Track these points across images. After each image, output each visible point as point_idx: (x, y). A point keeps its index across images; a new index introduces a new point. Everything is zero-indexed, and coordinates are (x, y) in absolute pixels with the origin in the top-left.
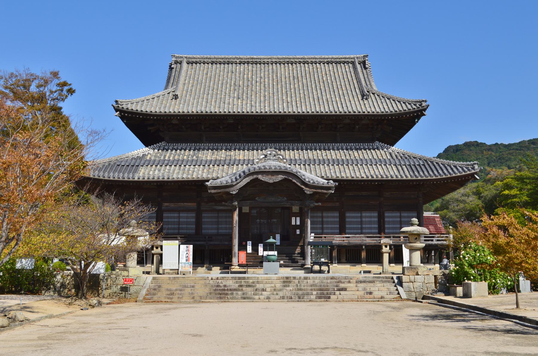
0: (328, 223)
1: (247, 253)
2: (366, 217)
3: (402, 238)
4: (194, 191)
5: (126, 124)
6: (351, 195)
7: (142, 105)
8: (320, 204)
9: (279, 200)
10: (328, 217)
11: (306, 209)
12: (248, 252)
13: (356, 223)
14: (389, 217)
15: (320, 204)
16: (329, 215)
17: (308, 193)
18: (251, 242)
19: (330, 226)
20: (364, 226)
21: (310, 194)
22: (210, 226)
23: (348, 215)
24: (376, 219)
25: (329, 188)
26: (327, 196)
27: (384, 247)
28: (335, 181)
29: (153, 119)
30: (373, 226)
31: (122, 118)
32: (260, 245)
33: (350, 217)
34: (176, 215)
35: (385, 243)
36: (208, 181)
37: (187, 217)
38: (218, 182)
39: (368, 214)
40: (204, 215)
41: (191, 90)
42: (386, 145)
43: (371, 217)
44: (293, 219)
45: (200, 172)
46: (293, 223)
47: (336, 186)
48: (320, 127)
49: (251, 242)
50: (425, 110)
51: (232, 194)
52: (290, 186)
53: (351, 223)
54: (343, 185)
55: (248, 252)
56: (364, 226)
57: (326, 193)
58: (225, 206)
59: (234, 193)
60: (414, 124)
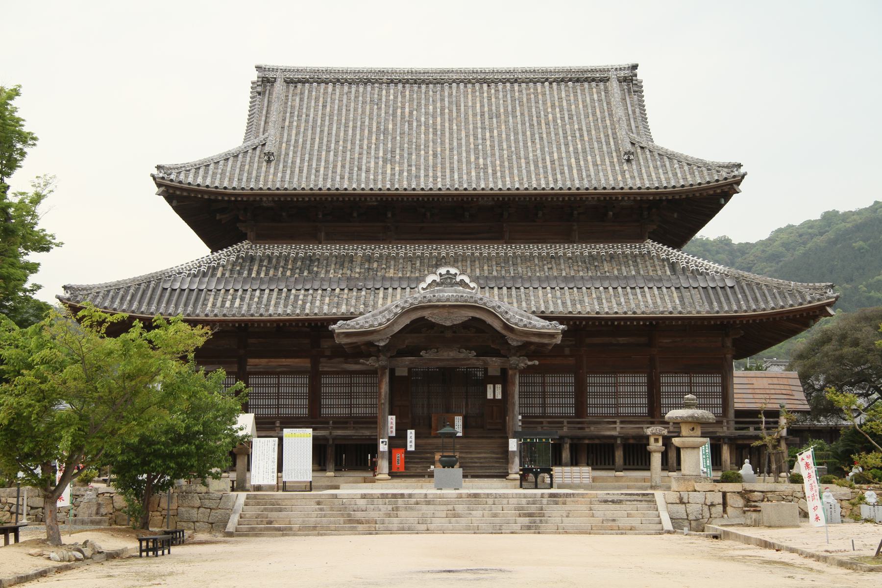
0: (553, 395)
1: (407, 452)
2: (625, 384)
3: (565, 424)
4: (306, 339)
5: (177, 209)
6: (593, 343)
7: (206, 172)
8: (537, 363)
9: (462, 356)
10: (553, 384)
11: (510, 372)
12: (409, 449)
13: (608, 395)
14: (669, 384)
15: (537, 363)
16: (557, 380)
17: (515, 344)
18: (413, 431)
19: (557, 401)
20: (621, 401)
21: (518, 347)
22: (335, 402)
23: (591, 380)
24: (644, 389)
25: (552, 336)
26: (550, 348)
27: (652, 440)
28: (561, 320)
29: (229, 201)
30: (638, 401)
31: (170, 198)
32: (409, 431)
33: (594, 385)
34: (273, 381)
35: (654, 434)
36: (335, 321)
37: (293, 386)
38: (353, 325)
39: (628, 379)
40: (324, 380)
41: (296, 141)
42: (665, 248)
43: (634, 384)
44: (490, 388)
45: (318, 303)
46: (490, 396)
47: (564, 332)
48: (540, 214)
49: (413, 431)
50: (738, 183)
51: (378, 346)
52: (480, 332)
53: (596, 395)
54: (581, 329)
55: (409, 449)
56: (621, 401)
57: (547, 344)
58: (363, 364)
59: (382, 344)
60: (720, 207)
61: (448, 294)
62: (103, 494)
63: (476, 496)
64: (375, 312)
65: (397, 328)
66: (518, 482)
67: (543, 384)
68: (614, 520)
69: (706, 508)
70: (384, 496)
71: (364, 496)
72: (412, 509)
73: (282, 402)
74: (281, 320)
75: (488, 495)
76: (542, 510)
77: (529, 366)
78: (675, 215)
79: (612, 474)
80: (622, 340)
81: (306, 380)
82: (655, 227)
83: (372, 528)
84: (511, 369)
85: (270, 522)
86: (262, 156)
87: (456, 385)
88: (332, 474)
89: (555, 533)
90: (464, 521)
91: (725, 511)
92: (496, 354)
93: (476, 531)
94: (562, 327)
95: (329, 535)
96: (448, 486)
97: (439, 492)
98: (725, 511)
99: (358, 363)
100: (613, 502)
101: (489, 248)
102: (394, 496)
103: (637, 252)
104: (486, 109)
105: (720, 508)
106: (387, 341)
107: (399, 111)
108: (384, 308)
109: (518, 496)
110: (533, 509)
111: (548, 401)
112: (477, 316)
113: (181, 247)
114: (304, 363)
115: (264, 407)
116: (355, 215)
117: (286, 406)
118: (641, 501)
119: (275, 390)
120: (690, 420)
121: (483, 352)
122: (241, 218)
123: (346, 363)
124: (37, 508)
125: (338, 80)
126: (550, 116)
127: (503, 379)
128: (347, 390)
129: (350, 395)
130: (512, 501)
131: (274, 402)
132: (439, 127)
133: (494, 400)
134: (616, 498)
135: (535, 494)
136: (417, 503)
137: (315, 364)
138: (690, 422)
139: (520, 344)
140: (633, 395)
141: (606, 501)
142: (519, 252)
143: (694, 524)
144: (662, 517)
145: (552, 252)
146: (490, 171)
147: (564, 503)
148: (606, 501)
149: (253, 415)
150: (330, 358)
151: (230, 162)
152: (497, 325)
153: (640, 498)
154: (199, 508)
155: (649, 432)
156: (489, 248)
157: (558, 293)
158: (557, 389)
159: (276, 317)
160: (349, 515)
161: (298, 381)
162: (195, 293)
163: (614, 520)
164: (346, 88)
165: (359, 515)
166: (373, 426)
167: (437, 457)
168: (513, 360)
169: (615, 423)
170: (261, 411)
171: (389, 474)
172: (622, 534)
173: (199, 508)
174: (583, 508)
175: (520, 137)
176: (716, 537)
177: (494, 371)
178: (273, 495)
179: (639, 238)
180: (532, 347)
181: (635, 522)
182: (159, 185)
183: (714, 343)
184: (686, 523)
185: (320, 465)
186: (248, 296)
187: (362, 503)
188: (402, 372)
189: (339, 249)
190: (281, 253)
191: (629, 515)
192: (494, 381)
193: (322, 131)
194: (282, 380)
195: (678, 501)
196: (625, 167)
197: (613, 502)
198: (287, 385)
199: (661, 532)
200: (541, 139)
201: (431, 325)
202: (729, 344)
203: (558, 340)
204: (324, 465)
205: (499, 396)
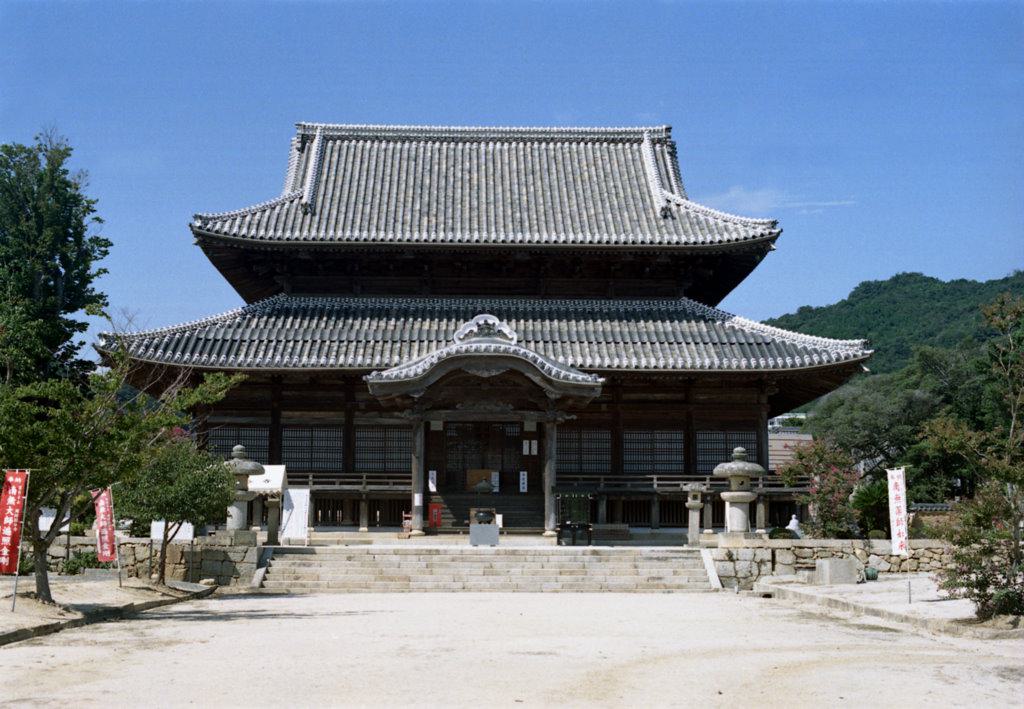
3: (761, 480)
8: (575, 417)
10: (590, 440)
11: (548, 426)
15: (575, 417)
17: (553, 396)
20: (658, 458)
22: (370, 456)
25: (592, 388)
28: (601, 373)
30: (674, 457)
34: (307, 434)
36: (369, 372)
42: (701, 305)
43: (670, 441)
44: (526, 444)
46: (526, 452)
47: (604, 385)
54: (618, 381)
56: (658, 458)
58: (398, 418)
60: (755, 264)
61: (483, 345)
62: (125, 544)
63: (514, 553)
64: (411, 362)
65: (433, 380)
66: (555, 540)
67: (580, 440)
68: (660, 578)
69: (755, 566)
70: (418, 553)
71: (396, 552)
72: (447, 566)
73: (315, 455)
74: (314, 371)
75: (526, 552)
76: (584, 567)
77: (567, 421)
78: (711, 272)
79: (648, 531)
80: (659, 396)
81: (266, 433)
82: (690, 284)
83: (406, 584)
84: (548, 422)
85: (297, 578)
86: (300, 207)
87: (491, 438)
88: (711, 531)
89: (599, 592)
90: (501, 580)
91: (773, 569)
92: (535, 407)
93: (517, 589)
94: (601, 380)
95: (361, 592)
96: (485, 542)
97: (475, 548)
98: (773, 569)
99: (392, 417)
100: (658, 559)
101: (526, 303)
102: (430, 552)
103: (672, 308)
104: (522, 166)
105: (769, 565)
106: (422, 394)
107: (436, 167)
108: (420, 358)
109: (560, 554)
110: (575, 566)
111: (585, 457)
112: (515, 368)
113: (221, 301)
114: (337, 417)
115: (297, 460)
116: (391, 267)
117: (319, 460)
118: (686, 558)
119: (308, 443)
120: (741, 473)
121: (522, 406)
122: (278, 270)
123: (381, 417)
124: (58, 558)
125: (377, 137)
126: (586, 174)
127: (540, 435)
128: (381, 444)
129: (383, 450)
130: (552, 558)
131: (308, 456)
132: (475, 182)
133: (530, 456)
134: (661, 555)
135: (577, 551)
136: (453, 560)
137: (350, 417)
138: (740, 476)
139: (558, 396)
140: (670, 451)
141: (651, 559)
142: (554, 308)
143: (743, 581)
144: (709, 574)
145: (588, 308)
146: (527, 224)
147: (607, 561)
148: (651, 559)
149: (903, 469)
150: (365, 411)
151: (267, 213)
152: (537, 379)
153: (685, 555)
154: (223, 562)
155: (685, 488)
156: (526, 303)
157: (595, 348)
158: (594, 446)
159: (309, 368)
160: (381, 572)
161: (333, 434)
162: (219, 343)
163: (660, 578)
164: (384, 145)
165: (392, 571)
166: (407, 481)
167: (473, 512)
168: (550, 415)
169: (362, 477)
170: (293, 465)
171: (424, 530)
172: (669, 592)
173: (223, 562)
174: (626, 566)
175: (556, 193)
176: (768, 596)
177: (530, 426)
178: (641, 551)
179: (672, 295)
180: (570, 402)
181: (681, 580)
182: (197, 235)
183: (749, 399)
184: (734, 581)
185: (353, 520)
186: (281, 347)
187: (395, 559)
188: (437, 426)
189: (375, 303)
190: (467, 308)
191: (675, 573)
192: (530, 436)
193: (359, 185)
194: (315, 434)
195: (727, 558)
196: (662, 223)
197: (658, 559)
198: (662, 441)
199: (709, 590)
200: (577, 195)
201: (469, 379)
202: (764, 400)
203: (598, 394)
204: (358, 520)
205: (535, 452)
